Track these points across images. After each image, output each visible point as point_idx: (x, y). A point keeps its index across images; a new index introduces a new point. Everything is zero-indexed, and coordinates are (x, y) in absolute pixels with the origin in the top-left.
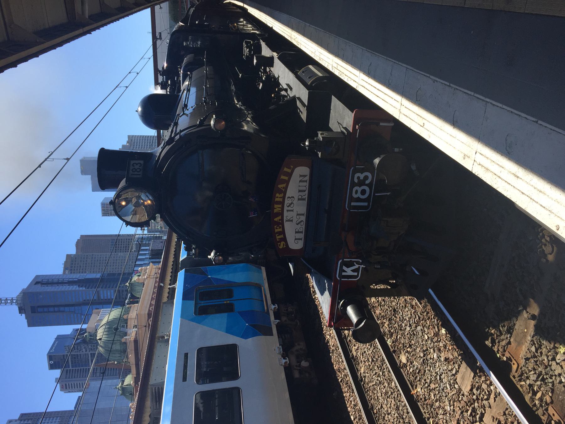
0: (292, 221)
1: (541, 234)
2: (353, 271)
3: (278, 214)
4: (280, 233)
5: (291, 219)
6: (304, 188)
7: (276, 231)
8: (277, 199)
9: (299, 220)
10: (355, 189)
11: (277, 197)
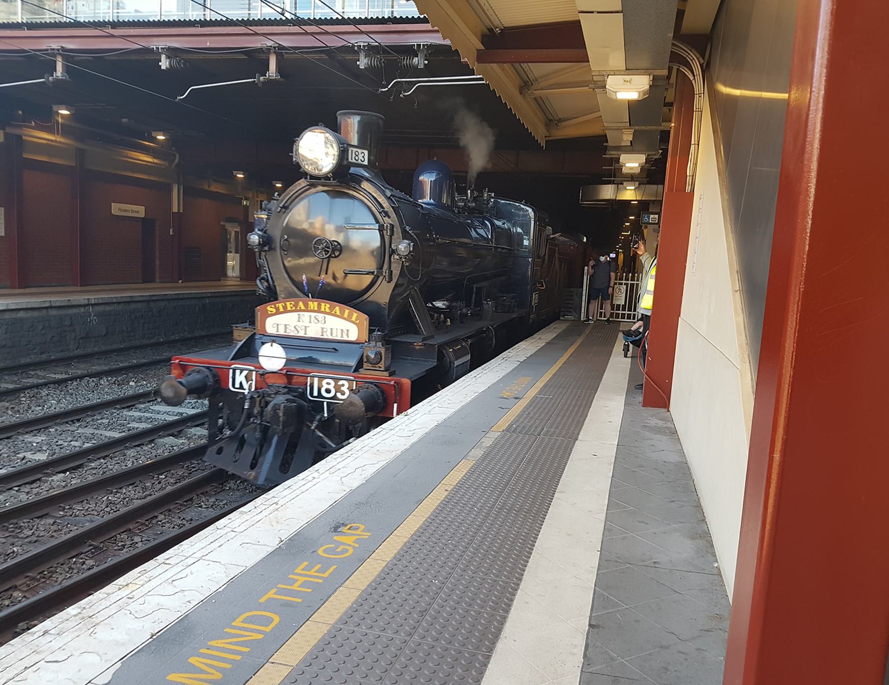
0: (299, 321)
1: (152, 380)
2: (241, 383)
3: (306, 305)
4: (285, 307)
5: (301, 320)
6: (334, 334)
7: (288, 304)
8: (323, 305)
9: (299, 329)
10: (332, 382)
11: (325, 305)
